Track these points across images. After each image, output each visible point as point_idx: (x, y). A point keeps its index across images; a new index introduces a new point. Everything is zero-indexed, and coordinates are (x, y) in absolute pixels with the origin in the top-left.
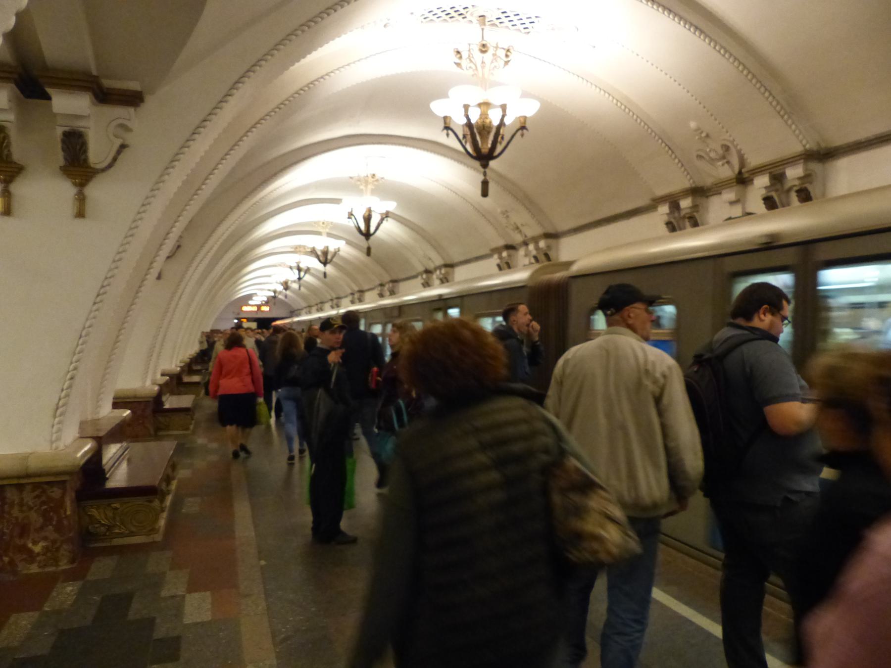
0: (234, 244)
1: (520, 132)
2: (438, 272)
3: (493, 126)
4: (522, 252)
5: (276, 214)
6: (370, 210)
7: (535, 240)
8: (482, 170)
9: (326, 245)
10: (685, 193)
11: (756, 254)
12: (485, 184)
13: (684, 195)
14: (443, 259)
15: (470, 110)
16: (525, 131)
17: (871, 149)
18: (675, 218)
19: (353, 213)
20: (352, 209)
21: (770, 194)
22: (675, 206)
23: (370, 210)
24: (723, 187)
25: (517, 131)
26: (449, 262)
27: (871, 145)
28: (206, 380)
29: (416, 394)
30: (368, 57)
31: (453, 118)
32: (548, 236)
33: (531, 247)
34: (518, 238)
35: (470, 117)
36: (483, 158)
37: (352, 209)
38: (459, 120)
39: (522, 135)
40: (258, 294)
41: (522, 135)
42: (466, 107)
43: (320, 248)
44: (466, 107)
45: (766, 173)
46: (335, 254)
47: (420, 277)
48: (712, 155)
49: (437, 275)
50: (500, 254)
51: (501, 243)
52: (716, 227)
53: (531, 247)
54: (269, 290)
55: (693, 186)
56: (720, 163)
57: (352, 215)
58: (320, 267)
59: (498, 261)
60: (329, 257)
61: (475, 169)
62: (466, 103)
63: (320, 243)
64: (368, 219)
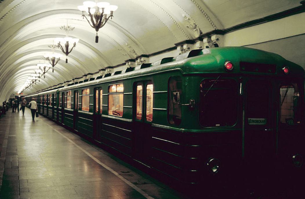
0: (20, 69)
1: (111, 17)
2: (139, 60)
5: (29, 61)
6: (68, 42)
9: (54, 57)
11: (102, 84)
14: (212, 24)
15: (91, 9)
16: (112, 17)
18: (209, 45)
19: (61, 44)
20: (60, 42)
23: (68, 42)
27: (262, 21)
29: (55, 108)
32: (217, 32)
35: (91, 12)
37: (60, 42)
39: (112, 18)
41: (112, 18)
42: (89, 8)
43: (51, 57)
44: (89, 8)
45: (206, 37)
46: (59, 59)
48: (191, 27)
49: (138, 63)
50: (182, 46)
52: (123, 74)
53: (205, 40)
56: (194, 30)
57: (60, 45)
58: (63, 57)
60: (70, 48)
62: (89, 7)
63: (51, 55)
64: (67, 46)
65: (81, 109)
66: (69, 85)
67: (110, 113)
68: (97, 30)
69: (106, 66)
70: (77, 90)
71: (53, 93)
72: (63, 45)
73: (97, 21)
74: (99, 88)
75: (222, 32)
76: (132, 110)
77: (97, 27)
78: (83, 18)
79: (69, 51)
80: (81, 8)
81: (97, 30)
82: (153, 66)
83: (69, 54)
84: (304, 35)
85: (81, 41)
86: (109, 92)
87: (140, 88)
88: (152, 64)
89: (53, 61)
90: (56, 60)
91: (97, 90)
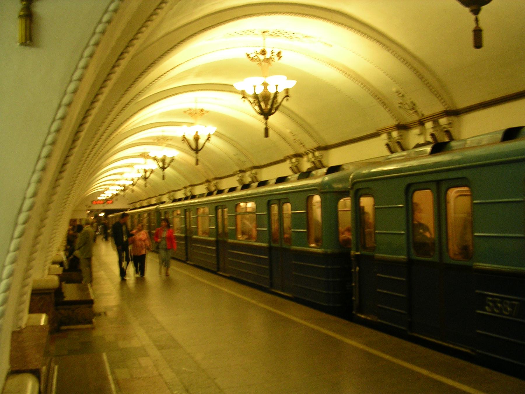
1: (286, 98)
3: (270, 94)
4: (305, 159)
7: (434, 119)
8: (195, 155)
10: (316, 149)
12: (197, 161)
13: (316, 150)
14: (394, 117)
17: (468, 114)
21: (434, 132)
22: (389, 134)
24: (427, 121)
25: (284, 98)
26: (322, 144)
28: (109, 200)
30: (198, 56)
31: (246, 91)
32: (448, 113)
33: (310, 156)
34: (302, 150)
36: (266, 114)
38: (250, 92)
40: (109, 188)
43: (160, 156)
46: (172, 160)
47: (288, 162)
51: (292, 152)
53: (310, 156)
54: (119, 185)
55: (295, 153)
59: (290, 165)
60: (201, 141)
61: (191, 156)
62: (254, 85)
64: (197, 139)
65: (197, 234)
66: (175, 201)
67: (285, 213)
68: (266, 118)
69: (188, 184)
70: (189, 209)
71: (166, 210)
72: (190, 137)
73: (266, 105)
74: (222, 206)
75: (327, 148)
76: (305, 215)
77: (266, 114)
78: (244, 101)
79: (200, 147)
80: (239, 85)
81: (266, 118)
82: (417, 135)
83: (200, 152)
84: (39, 9)
85: (218, 135)
86: (236, 211)
87: (275, 208)
88: (289, 178)
89: (163, 161)
90: (167, 161)
91: (220, 209)
